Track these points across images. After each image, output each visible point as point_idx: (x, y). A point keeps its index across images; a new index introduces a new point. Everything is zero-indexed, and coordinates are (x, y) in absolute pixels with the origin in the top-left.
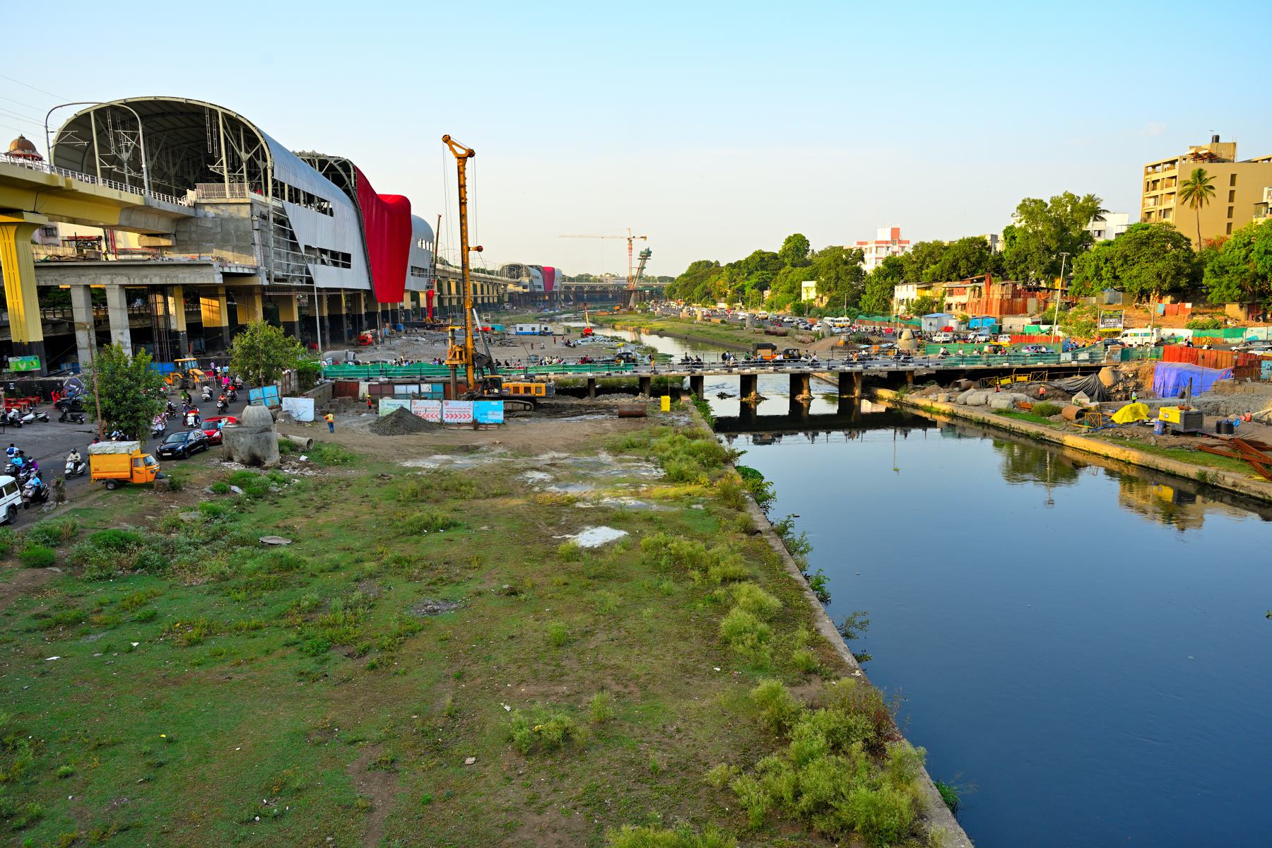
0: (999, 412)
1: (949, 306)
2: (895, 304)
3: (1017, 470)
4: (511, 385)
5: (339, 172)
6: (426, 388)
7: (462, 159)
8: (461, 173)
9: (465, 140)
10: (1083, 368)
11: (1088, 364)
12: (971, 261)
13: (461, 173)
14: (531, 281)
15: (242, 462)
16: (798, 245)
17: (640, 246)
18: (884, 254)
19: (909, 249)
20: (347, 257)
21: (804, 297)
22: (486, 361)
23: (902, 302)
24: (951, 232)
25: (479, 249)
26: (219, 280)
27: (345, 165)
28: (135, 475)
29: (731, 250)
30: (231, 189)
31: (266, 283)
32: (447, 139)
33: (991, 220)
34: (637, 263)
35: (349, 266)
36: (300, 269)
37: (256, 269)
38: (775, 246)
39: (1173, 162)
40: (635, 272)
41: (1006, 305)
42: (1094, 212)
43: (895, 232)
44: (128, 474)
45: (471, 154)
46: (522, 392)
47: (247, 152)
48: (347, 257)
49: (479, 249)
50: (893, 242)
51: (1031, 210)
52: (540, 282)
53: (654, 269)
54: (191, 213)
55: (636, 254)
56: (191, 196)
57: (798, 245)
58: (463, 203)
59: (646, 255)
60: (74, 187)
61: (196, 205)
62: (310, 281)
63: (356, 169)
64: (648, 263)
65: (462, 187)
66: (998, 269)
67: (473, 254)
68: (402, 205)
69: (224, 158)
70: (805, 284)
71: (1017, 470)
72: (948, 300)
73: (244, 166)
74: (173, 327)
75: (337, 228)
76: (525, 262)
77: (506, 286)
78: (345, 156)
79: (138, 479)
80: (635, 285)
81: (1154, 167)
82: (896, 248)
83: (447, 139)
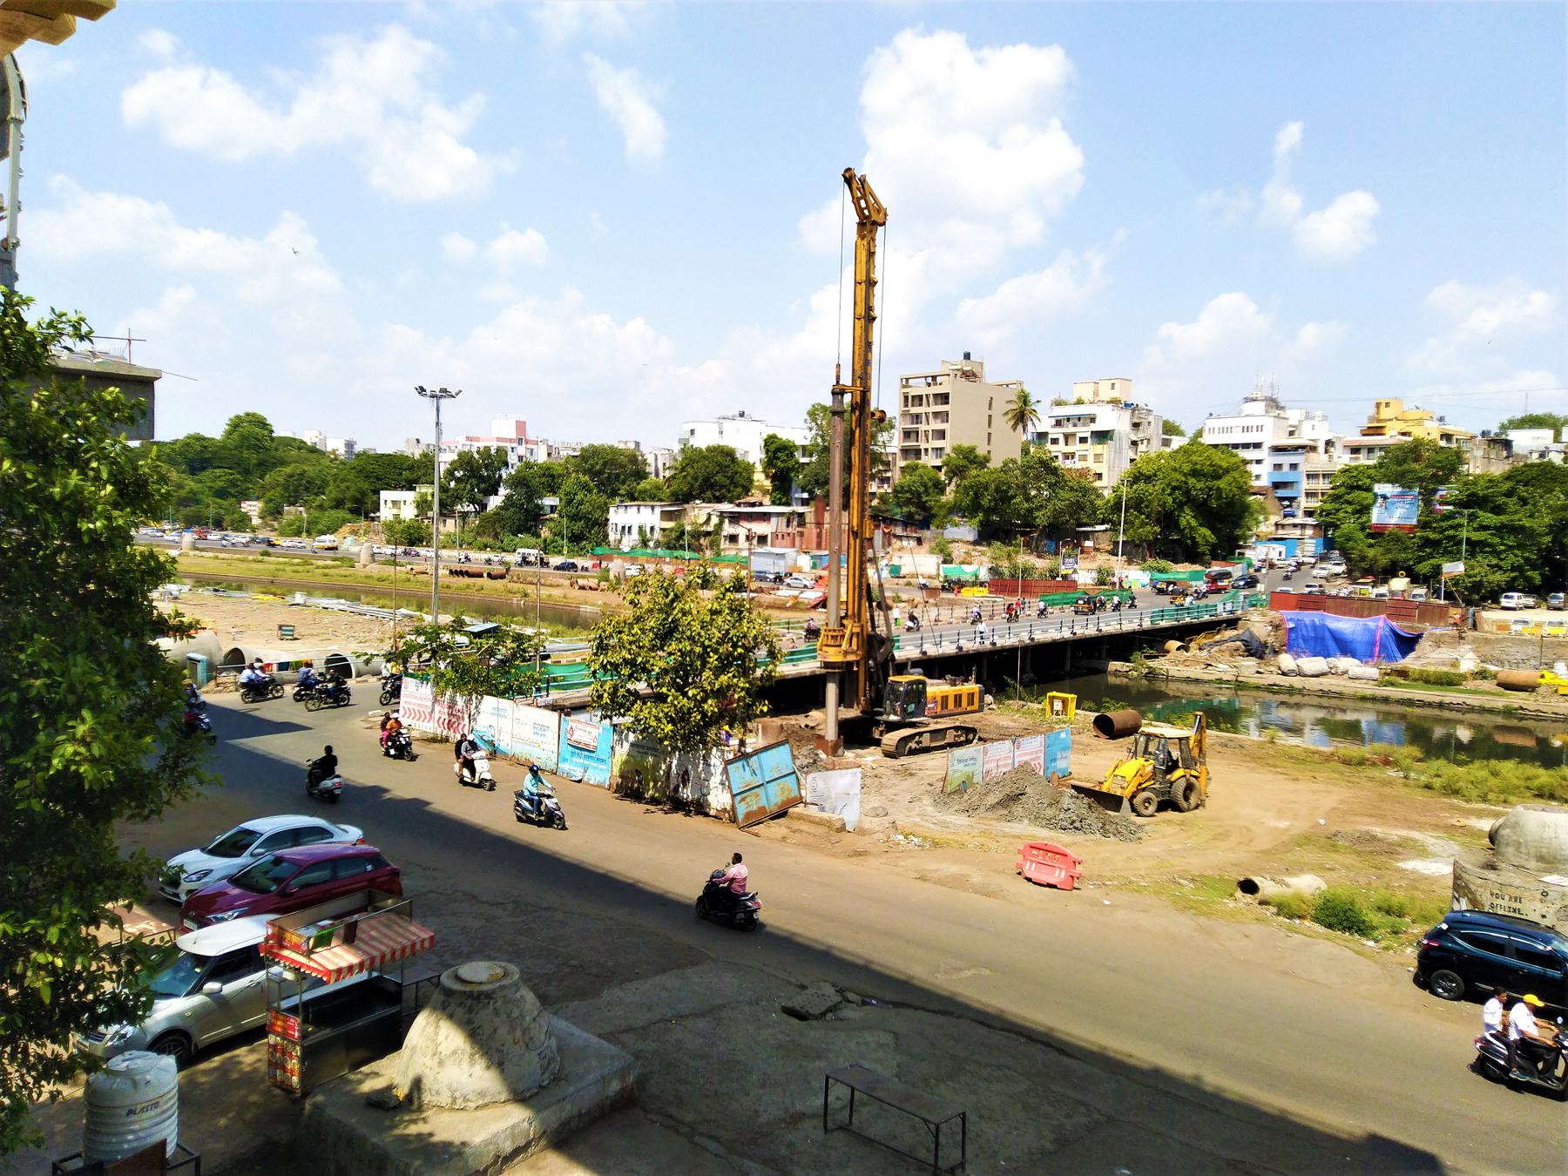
43: (521, 426)
50: (520, 441)
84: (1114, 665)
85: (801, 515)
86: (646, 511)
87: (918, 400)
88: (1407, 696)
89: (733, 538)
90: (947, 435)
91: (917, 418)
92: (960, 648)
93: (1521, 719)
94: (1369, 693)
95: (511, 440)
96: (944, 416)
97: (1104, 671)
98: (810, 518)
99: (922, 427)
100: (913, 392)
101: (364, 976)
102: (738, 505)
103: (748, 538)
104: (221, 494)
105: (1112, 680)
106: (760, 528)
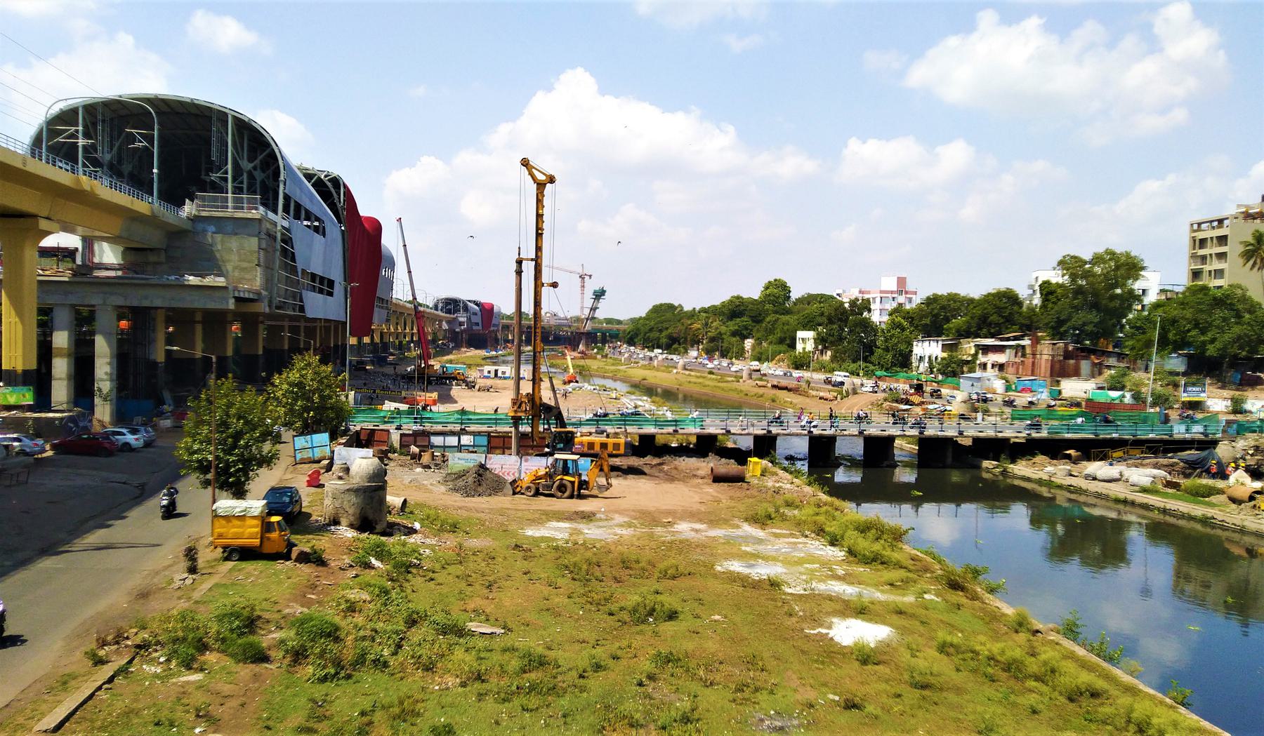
0: (1144, 490)
1: (984, 366)
2: (914, 360)
3: (1061, 551)
4: (586, 439)
5: (331, 189)
6: (466, 440)
7: (541, 186)
8: (539, 202)
9: (545, 165)
10: (1200, 442)
11: (1202, 437)
12: (998, 316)
13: (539, 202)
14: (469, 319)
15: (351, 526)
16: (777, 292)
17: (592, 286)
18: (891, 306)
19: (917, 300)
20: (331, 283)
21: (799, 347)
22: (555, 412)
23: (921, 359)
24: (975, 286)
25: (555, 285)
26: (231, 305)
27: (336, 182)
28: (266, 543)
29: (699, 293)
30: (236, 200)
31: (267, 310)
32: (525, 163)
33: (1028, 273)
34: (589, 303)
35: (331, 294)
36: (294, 296)
37: (259, 294)
38: (753, 291)
39: (1221, 221)
40: (587, 312)
41: (1057, 366)
42: (1132, 267)
43: (901, 281)
44: (257, 542)
45: (552, 180)
46: (597, 448)
47: (250, 160)
48: (331, 283)
49: (555, 285)
50: (900, 292)
51: (1070, 264)
52: (478, 319)
53: (605, 311)
54: (188, 226)
55: (589, 295)
56: (189, 209)
57: (777, 292)
58: (539, 235)
59: (599, 294)
60: (97, 192)
61: (195, 219)
62: (302, 309)
63: (345, 186)
64: (602, 304)
65: (539, 217)
66: (1028, 325)
67: (545, 291)
68: (376, 227)
69: (230, 166)
70: (800, 334)
71: (1061, 551)
72: (982, 359)
73: (245, 176)
74: (152, 357)
75: (322, 253)
76: (463, 295)
77: (441, 321)
78: (336, 171)
79: (267, 549)
80: (589, 327)
81: (1199, 224)
82: (901, 299)
83: (525, 163)
84: (986, 464)
85: (1023, 347)
86: (933, 344)
87: (1203, 243)
88: (1145, 501)
89: (984, 366)
90: (1226, 274)
91: (1203, 259)
92: (769, 432)
93: (1213, 528)
94: (1122, 496)
95: (892, 292)
96: (1222, 256)
97: (979, 467)
98: (1028, 351)
99: (1207, 268)
100: (1200, 235)
101: (120, 273)
102: (1002, 339)
103: (993, 366)
104: (734, 334)
105: (985, 475)
106: (1001, 358)
